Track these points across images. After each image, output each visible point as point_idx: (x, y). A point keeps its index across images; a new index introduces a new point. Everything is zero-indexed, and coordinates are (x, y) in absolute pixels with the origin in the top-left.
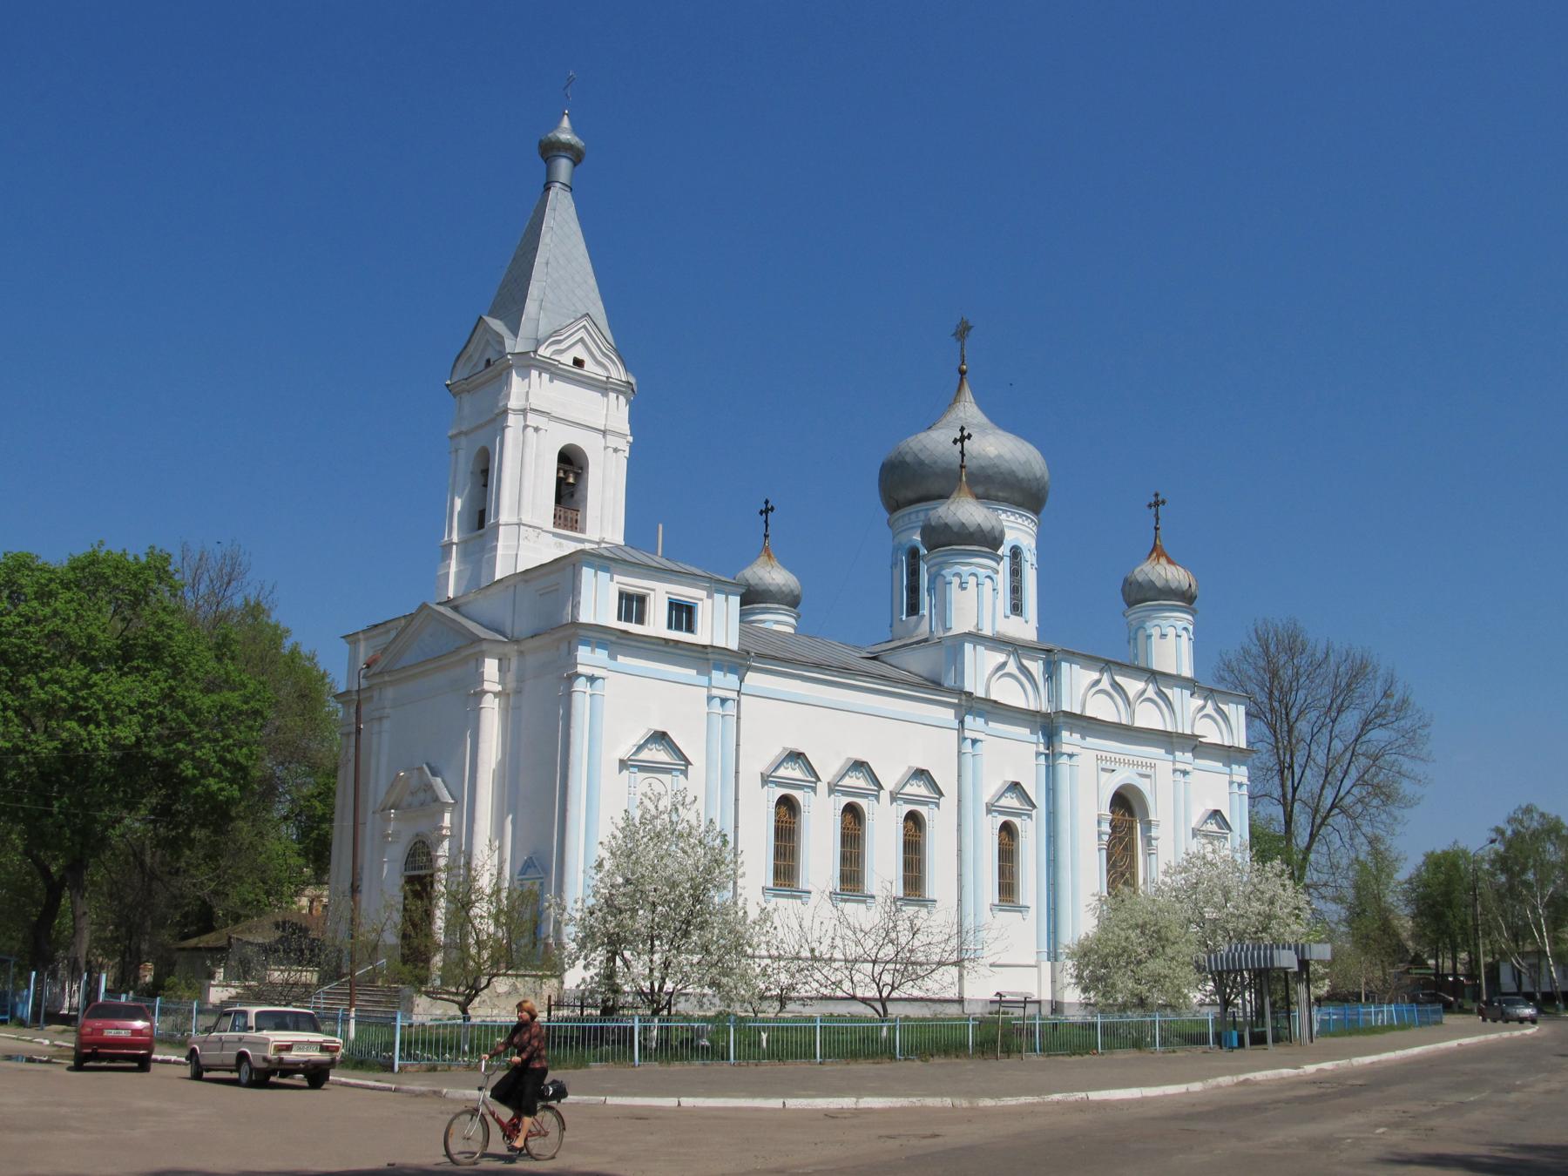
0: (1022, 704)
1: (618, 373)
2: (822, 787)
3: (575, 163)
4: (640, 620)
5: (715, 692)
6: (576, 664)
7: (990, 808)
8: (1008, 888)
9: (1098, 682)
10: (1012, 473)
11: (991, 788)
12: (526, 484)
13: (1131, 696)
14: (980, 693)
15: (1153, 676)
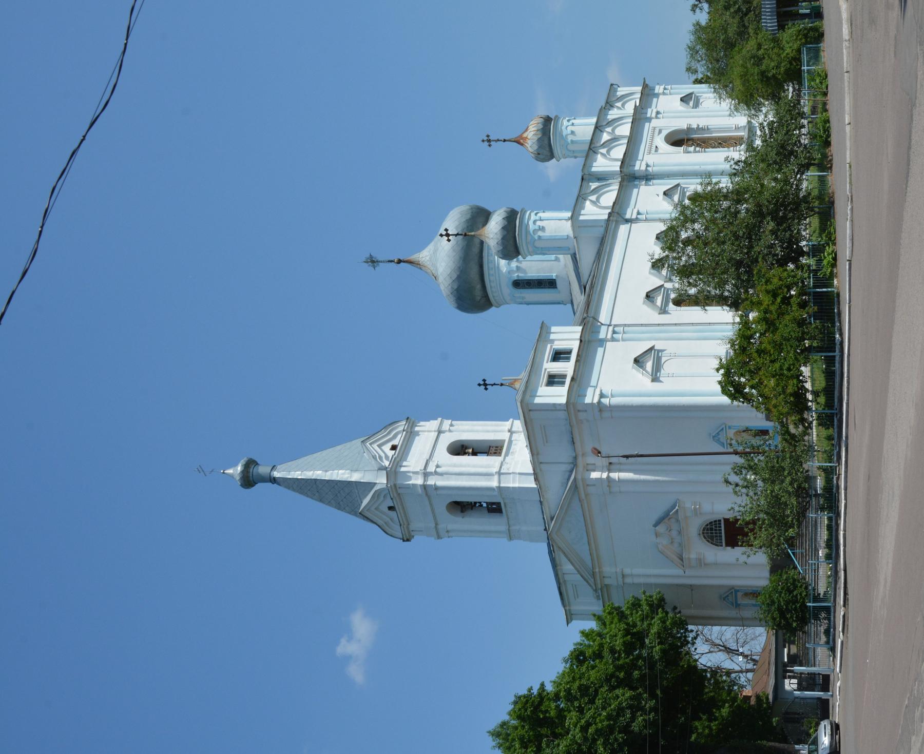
1: (402, 426)
5: (609, 336)
6: (592, 404)
10: (468, 221)
12: (473, 470)
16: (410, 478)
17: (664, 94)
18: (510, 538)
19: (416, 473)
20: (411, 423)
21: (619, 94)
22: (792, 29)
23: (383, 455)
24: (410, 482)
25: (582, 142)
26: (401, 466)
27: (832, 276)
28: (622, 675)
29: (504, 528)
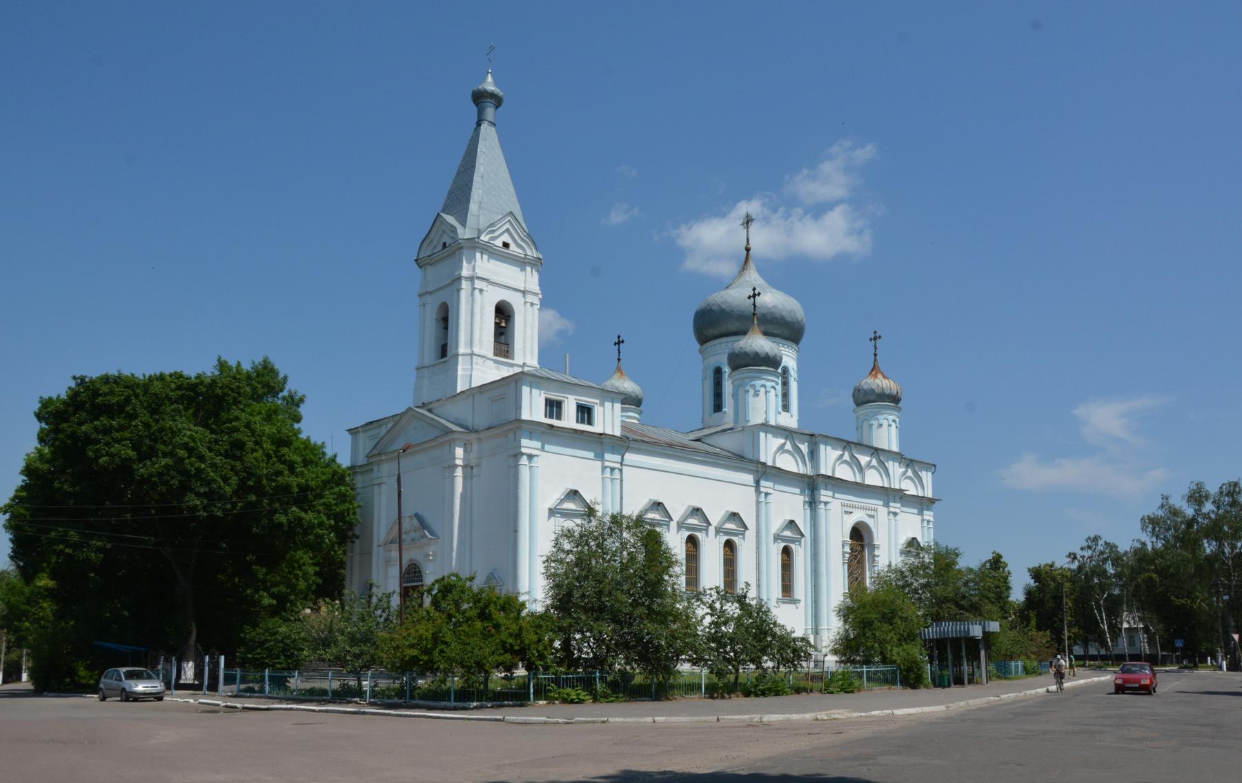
0: (795, 470)
1: (532, 253)
2: (712, 530)
3: (497, 106)
4: (559, 417)
5: (607, 464)
6: (520, 447)
7: (777, 538)
8: (787, 588)
9: (842, 456)
10: (783, 318)
11: (776, 524)
14: (770, 463)
15: (876, 452)
16: (469, 262)
17: (923, 520)
18: (418, 369)
19: (474, 269)
20: (535, 263)
21: (923, 474)
22: (917, 652)
23: (496, 234)
24: (465, 263)
25: (870, 436)
27: (551, 700)
28: (250, 483)
29: (427, 362)
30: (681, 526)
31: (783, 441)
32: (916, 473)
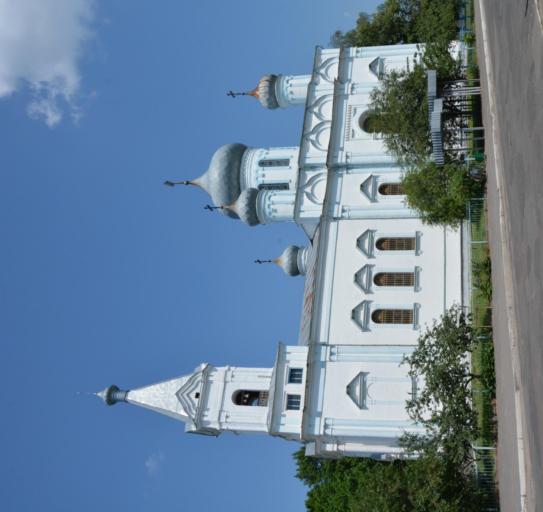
4: (299, 397)
5: (328, 359)
11: (364, 200)
13: (320, 122)
17: (357, 57)
26: (204, 416)
30: (368, 291)
31: (314, 116)
32: (323, 66)
